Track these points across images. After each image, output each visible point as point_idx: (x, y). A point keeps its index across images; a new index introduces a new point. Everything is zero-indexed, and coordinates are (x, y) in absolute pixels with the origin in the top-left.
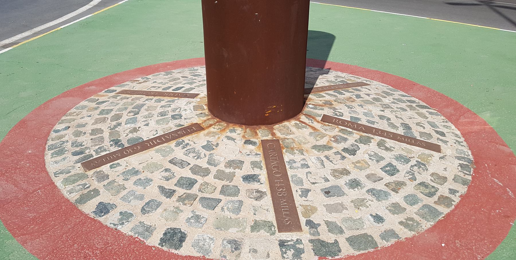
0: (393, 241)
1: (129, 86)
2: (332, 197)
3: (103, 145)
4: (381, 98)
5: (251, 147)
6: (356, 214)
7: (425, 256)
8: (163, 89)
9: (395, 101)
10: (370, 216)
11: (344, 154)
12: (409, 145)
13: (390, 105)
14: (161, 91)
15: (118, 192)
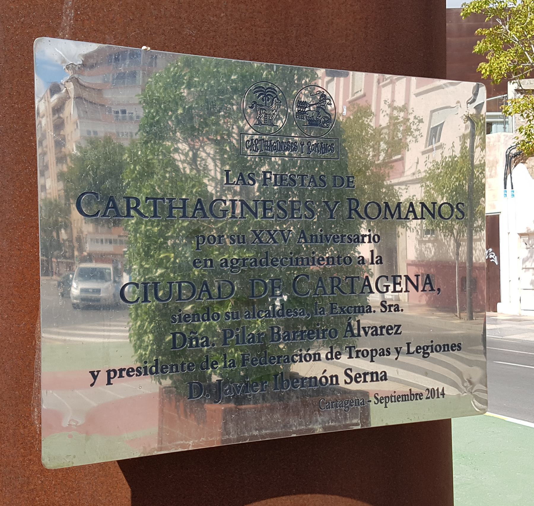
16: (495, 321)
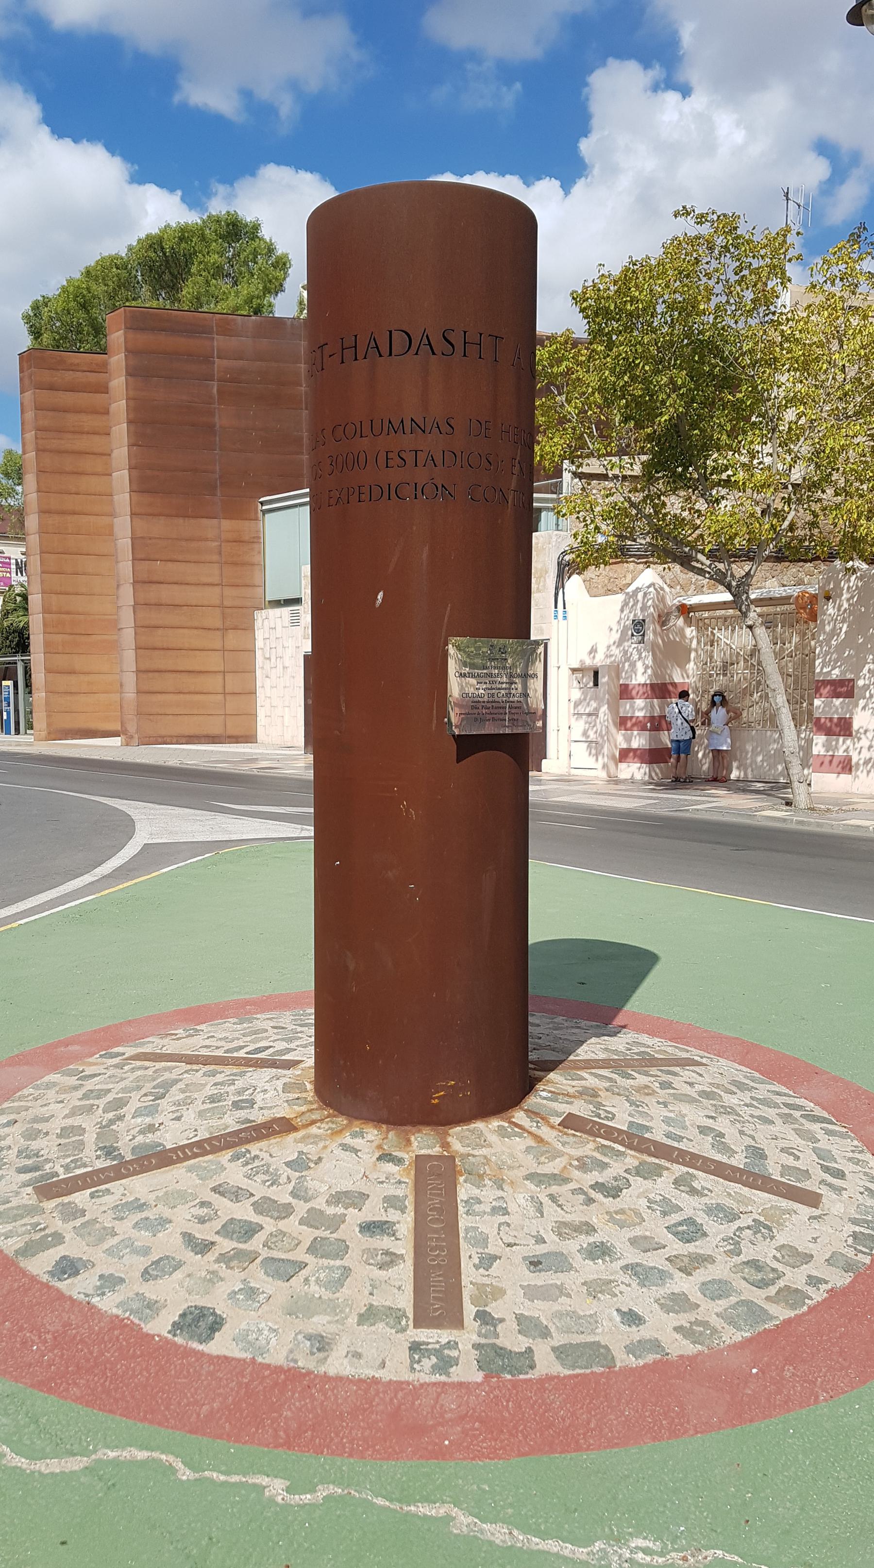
0: (650, 1358)
1: (154, 1044)
2: (543, 1273)
3: (80, 1156)
4: (722, 1093)
5: (390, 1167)
6: (586, 1307)
7: (709, 1387)
8: (227, 1051)
9: (755, 1103)
10: (615, 1313)
11: (593, 1194)
12: (746, 1189)
13: (738, 1109)
14: (221, 1054)
15: (101, 1240)
16: (539, 782)
